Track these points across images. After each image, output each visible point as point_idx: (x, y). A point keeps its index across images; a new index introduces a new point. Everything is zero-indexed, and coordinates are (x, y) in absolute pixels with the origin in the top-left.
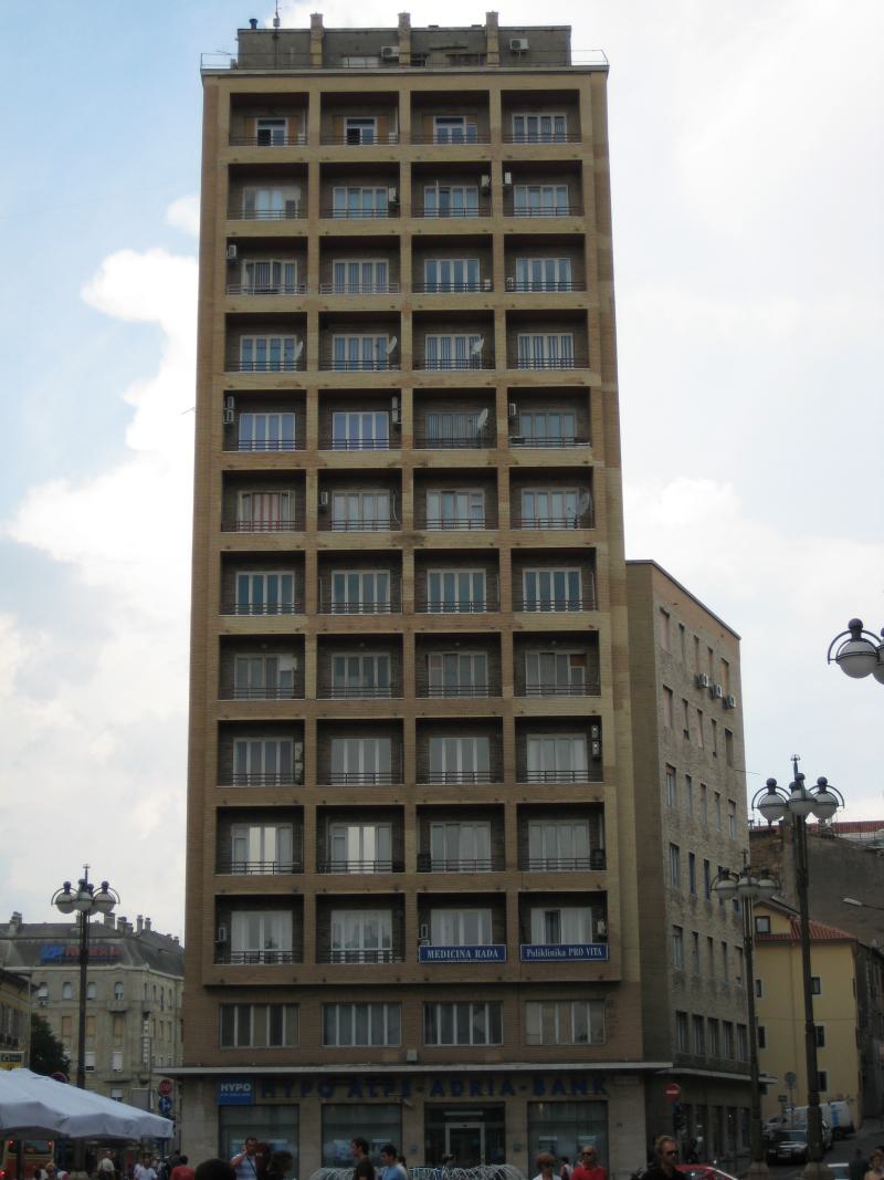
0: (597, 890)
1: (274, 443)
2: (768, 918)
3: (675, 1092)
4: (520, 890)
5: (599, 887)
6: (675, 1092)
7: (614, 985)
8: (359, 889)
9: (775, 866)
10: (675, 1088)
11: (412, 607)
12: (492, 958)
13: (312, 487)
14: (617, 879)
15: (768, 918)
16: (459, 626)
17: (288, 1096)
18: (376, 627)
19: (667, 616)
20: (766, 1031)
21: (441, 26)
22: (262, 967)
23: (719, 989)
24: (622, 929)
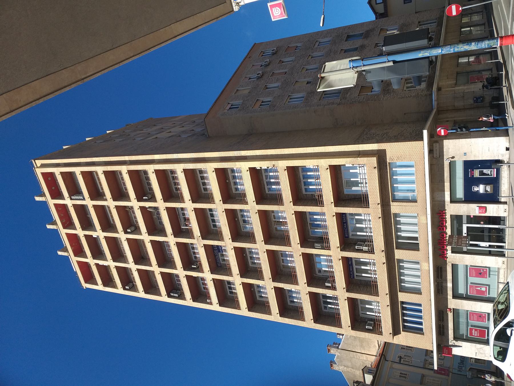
6: (442, 131)
10: (440, 131)
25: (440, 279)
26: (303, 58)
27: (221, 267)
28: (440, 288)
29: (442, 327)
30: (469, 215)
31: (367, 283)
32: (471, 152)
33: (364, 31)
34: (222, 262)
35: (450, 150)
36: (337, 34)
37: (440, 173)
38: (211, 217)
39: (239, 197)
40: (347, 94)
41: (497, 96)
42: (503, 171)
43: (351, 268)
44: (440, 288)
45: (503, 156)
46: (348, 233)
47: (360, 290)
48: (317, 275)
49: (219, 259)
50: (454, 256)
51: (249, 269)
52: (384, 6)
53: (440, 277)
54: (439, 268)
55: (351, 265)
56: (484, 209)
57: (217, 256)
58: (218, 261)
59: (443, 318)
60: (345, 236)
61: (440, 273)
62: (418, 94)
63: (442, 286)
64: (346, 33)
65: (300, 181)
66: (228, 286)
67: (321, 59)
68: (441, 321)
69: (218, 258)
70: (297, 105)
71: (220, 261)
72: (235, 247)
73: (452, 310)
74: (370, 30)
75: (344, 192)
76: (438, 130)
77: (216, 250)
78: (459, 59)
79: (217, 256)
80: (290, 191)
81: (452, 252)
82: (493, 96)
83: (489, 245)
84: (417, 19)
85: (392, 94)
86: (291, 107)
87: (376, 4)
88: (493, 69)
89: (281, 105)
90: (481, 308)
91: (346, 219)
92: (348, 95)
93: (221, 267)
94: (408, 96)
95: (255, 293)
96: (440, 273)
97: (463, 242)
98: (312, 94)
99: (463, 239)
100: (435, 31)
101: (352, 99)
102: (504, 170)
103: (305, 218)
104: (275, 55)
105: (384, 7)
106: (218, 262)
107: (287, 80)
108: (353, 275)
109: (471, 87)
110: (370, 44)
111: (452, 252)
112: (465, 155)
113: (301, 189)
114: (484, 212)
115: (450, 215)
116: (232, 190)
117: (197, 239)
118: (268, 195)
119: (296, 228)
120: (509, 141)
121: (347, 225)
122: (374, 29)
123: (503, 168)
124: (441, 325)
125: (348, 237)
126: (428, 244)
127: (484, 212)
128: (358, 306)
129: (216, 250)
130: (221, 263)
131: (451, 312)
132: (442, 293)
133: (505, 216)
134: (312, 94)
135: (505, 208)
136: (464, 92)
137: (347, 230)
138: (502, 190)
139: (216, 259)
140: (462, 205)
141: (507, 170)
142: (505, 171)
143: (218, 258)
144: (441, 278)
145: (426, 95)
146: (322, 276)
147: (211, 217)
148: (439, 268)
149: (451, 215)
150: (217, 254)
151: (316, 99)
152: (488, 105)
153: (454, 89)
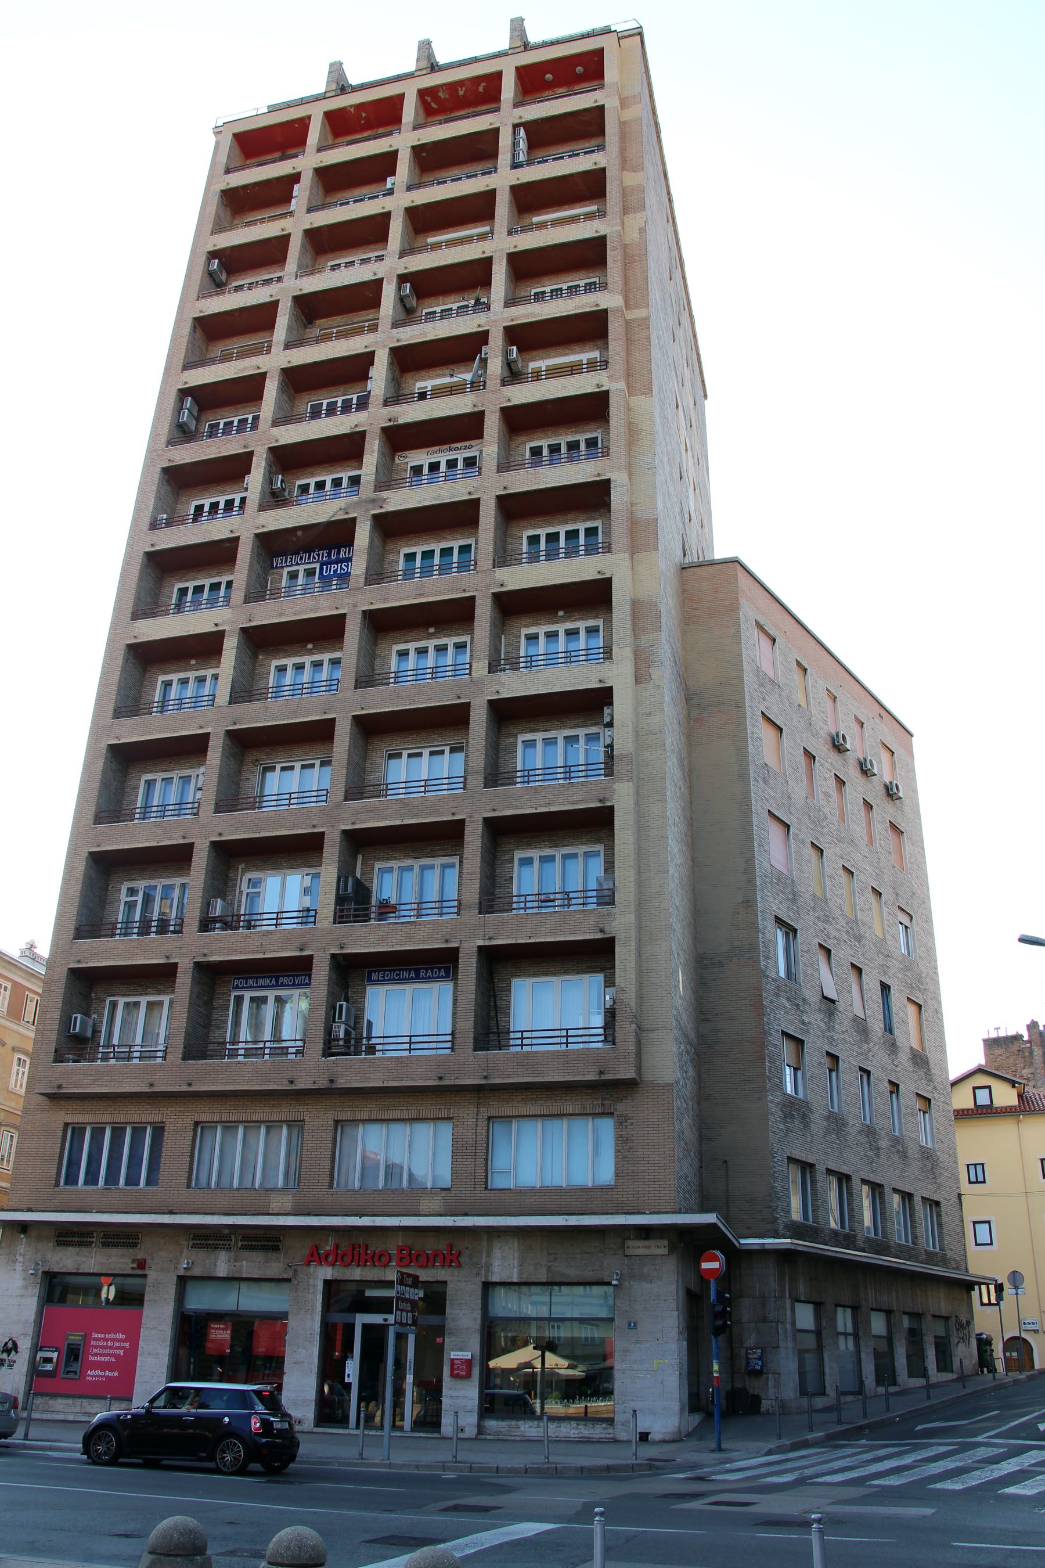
0: (599, 936)
1: (568, 770)
2: (989, 1087)
3: (715, 1265)
4: (481, 943)
5: (602, 931)
6: (715, 1265)
7: (627, 1087)
8: (253, 953)
9: (1025, 1072)
10: (715, 1259)
11: (362, 580)
12: (297, 976)
13: (257, 468)
14: (632, 918)
15: (989, 1087)
16: (421, 595)
17: (964, 1387)
18: (312, 610)
19: (835, 699)
20: (418, 759)
21: (707, 403)
22: (136, 1065)
23: (884, 1143)
24: (640, 997)
25: (240, 1244)
26: (874, 874)
27: (272, 567)
28: (210, 1242)
29: (85, 1239)
30: (447, 1332)
31: (219, 1028)
32: (637, 1342)
33: (928, 1054)
34: (288, 572)
35: (646, 1286)
36: (924, 975)
37: (578, 1256)
38: (441, 550)
39: (505, 646)
40: (788, 999)
41: (763, 1409)
42: (578, 1425)
43: (268, 981)
44: (210, 1242)
45: (623, 1425)
46: (385, 980)
47: (198, 1006)
48: (243, 874)
49: (297, 564)
50: (315, 1286)
51: (261, 657)
52: (968, 1110)
53: (89, 1240)
54: (276, 1244)
55: (277, 981)
56: (464, 1373)
57: (309, 558)
58: (292, 559)
59: (116, 1245)
60: (375, 972)
61: (260, 1243)
62: (779, 1198)
63: (216, 1247)
64: (925, 1001)
65: (556, 846)
66: (204, 586)
67: (870, 928)
68: (103, 1240)
69: (301, 559)
70: (765, 851)
71: (292, 565)
72: (345, 619)
73: (140, 1272)
74: (929, 1069)
75: (519, 976)
76: (718, 1253)
77: (329, 555)
78: (811, 1307)
79: (309, 558)
80: (533, 811)
81: (327, 1283)
82: (763, 1397)
83: (350, 1384)
84: (946, 1199)
85: (782, 1126)
86: (763, 832)
87: (974, 1088)
88: (825, 1399)
89: (767, 800)
90: (149, 1354)
91: (429, 977)
92: (784, 1001)
93: (272, 567)
94: (775, 1172)
95: (181, 671)
96: (260, 1243)
97: (404, 1314)
98: (791, 897)
99: (410, 1315)
100: (916, 1244)
101: (776, 1014)
102: (580, 1427)
103: (432, 850)
104: (884, 791)
105: (963, 1110)
106: (289, 560)
107: (825, 824)
108: (243, 987)
109: (789, 1339)
110: (898, 1069)
111: (327, 1283)
112: (630, 1325)
113: (529, 846)
114: (456, 1372)
115: (445, 1279)
116: (533, 625)
117: (373, 501)
118: (511, 740)
119: (406, 822)
120: (666, 1438)
121: (409, 979)
122: (931, 1080)
123: (586, 1425)
124: (91, 1240)
125: (370, 980)
126: (361, 1215)
127: (456, 1372)
128: (141, 994)
129: (329, 555)
130: (283, 567)
131: (133, 1268)
132: (194, 1246)
133: (443, 1429)
134: (791, 897)
135: (467, 1429)
136: (778, 1321)
137: (394, 979)
138: (520, 1423)
139: (299, 554)
140: (478, 1314)
141: (580, 1435)
142: (577, 1432)
143: (301, 559)
144: (243, 1247)
145: (775, 1220)
146: (237, 892)
147: (441, 550)
148: (276, 1244)
149: (446, 1282)
150: (314, 557)
151: (779, 909)
152: (738, 1385)
153: (787, 1296)
